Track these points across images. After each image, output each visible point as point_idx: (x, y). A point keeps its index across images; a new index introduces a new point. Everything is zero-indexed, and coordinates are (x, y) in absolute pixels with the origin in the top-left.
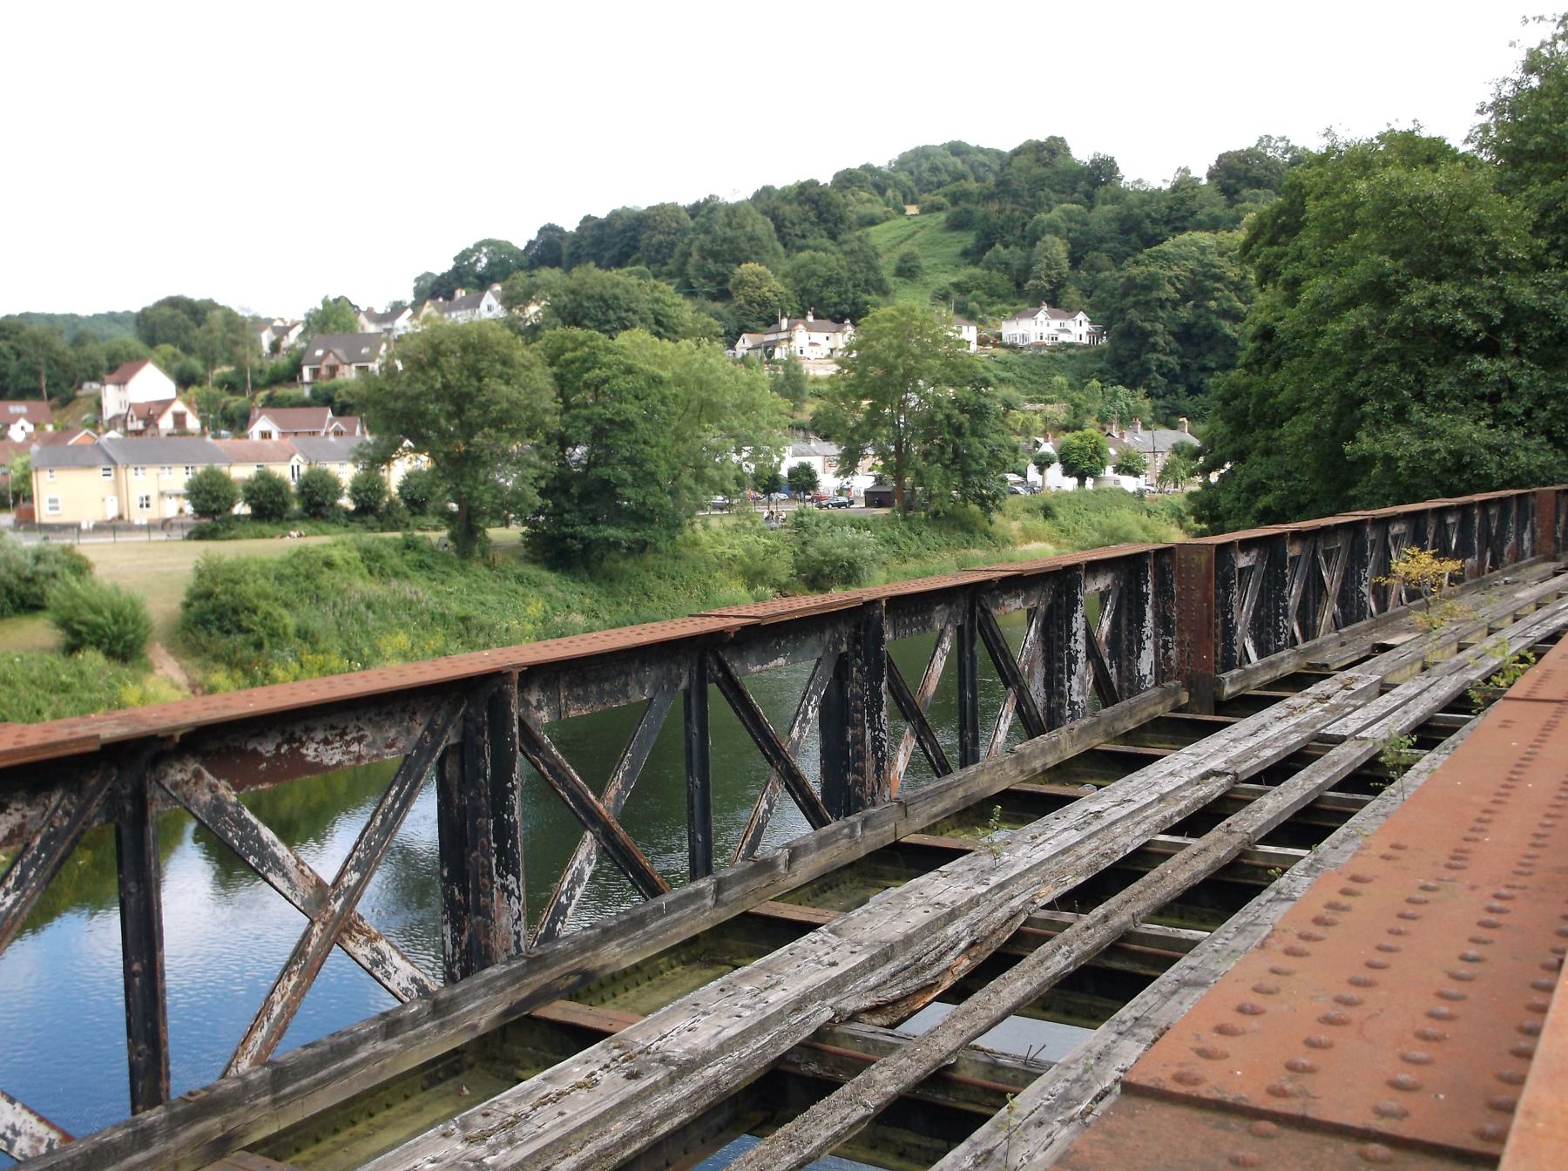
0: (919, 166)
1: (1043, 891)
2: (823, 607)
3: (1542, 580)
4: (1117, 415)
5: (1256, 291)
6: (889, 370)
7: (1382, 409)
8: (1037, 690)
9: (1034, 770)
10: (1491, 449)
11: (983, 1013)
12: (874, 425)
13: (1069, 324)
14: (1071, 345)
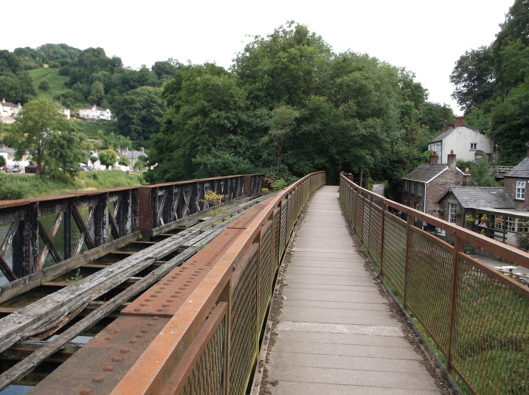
0: (49, 50)
1: (94, 295)
2: (16, 204)
3: (246, 202)
4: (120, 145)
5: (166, 108)
6: (36, 123)
7: (203, 149)
8: (92, 234)
9: (91, 260)
10: (234, 162)
11: (73, 332)
12: (29, 143)
13: (104, 113)
14: (104, 120)
